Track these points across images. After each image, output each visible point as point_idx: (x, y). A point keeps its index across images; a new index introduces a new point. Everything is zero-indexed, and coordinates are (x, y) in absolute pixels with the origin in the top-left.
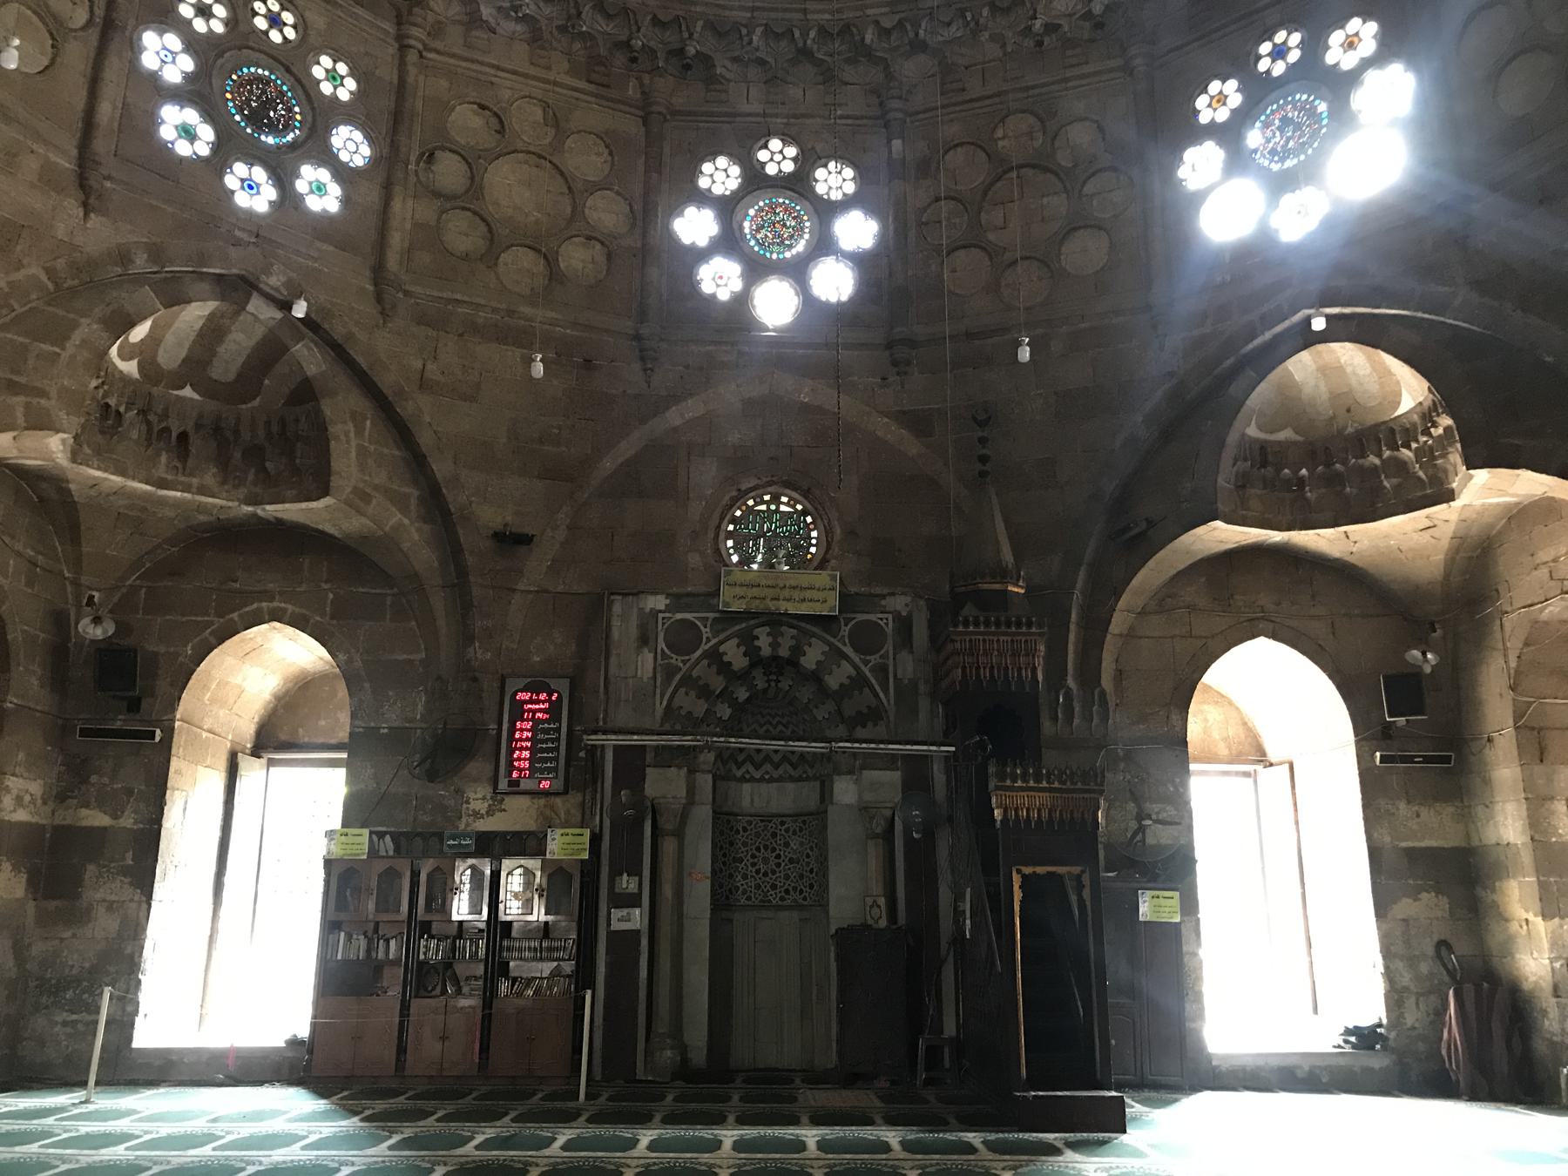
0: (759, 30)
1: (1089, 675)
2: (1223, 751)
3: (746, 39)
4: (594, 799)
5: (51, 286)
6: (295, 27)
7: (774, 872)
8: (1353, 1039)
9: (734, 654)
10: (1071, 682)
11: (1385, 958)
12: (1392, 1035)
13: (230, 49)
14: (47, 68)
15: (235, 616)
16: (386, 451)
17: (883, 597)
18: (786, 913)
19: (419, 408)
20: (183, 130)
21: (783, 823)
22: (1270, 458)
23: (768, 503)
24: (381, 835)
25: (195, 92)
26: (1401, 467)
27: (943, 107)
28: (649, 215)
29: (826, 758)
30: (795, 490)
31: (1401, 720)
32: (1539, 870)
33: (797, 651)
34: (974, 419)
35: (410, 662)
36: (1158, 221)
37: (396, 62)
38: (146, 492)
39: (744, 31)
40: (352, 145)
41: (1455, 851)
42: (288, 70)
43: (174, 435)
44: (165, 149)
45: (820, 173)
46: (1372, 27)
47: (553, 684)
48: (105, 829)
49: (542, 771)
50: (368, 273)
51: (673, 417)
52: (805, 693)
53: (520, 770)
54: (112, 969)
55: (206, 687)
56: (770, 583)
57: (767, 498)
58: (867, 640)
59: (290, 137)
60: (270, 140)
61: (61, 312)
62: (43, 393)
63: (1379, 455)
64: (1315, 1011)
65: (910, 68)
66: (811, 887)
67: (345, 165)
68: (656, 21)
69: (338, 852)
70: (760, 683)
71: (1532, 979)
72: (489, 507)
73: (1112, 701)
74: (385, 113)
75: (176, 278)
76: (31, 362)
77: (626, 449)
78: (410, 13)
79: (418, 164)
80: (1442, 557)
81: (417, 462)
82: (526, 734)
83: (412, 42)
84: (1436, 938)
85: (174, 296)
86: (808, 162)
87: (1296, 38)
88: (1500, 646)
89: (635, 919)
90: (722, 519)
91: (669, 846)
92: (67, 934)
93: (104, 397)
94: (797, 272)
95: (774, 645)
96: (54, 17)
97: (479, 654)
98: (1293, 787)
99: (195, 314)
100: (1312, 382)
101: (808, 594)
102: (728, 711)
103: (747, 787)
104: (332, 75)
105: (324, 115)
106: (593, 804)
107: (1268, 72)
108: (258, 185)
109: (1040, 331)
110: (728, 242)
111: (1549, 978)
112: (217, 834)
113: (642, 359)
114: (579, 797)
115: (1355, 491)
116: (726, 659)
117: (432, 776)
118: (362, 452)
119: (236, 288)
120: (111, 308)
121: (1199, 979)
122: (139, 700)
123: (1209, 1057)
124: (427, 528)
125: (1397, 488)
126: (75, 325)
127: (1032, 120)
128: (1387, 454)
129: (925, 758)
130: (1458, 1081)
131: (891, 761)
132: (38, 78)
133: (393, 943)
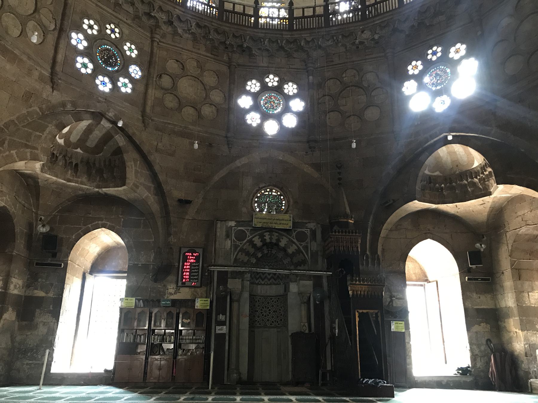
0: (267, 40)
1: (374, 250)
2: (414, 278)
3: (263, 43)
4: (210, 289)
5: (41, 113)
6: (119, 33)
7: (268, 315)
8: (460, 372)
9: (257, 241)
10: (368, 253)
11: (470, 344)
12: (473, 370)
13: (99, 39)
14: (41, 43)
15: (90, 226)
16: (144, 171)
17: (306, 223)
18: (273, 329)
19: (156, 159)
20: (84, 65)
21: (271, 299)
22: (432, 181)
23: (269, 192)
24: (139, 300)
25: (87, 53)
26: (474, 184)
27: (327, 66)
28: (230, 97)
29: (287, 276)
30: (278, 188)
31: (474, 266)
32: (520, 316)
33: (278, 240)
34: (337, 166)
35: (149, 242)
36: (395, 104)
37: (150, 45)
38: (63, 183)
39: (262, 40)
40: (135, 71)
41: (491, 309)
42: (117, 47)
43: (74, 164)
44: (78, 70)
45: (286, 86)
46: (464, 46)
47: (197, 250)
48: (43, 297)
49: (193, 279)
50: (140, 113)
51: (238, 163)
52: (280, 255)
53: (186, 279)
54: (44, 345)
55: (78, 250)
56: (270, 218)
57: (268, 190)
58: (301, 237)
59: (116, 68)
60: (110, 69)
61: (43, 122)
62: (37, 149)
63: (467, 180)
64: (446, 363)
65: (315, 54)
66: (281, 320)
67: (133, 78)
68: (234, 36)
69: (124, 305)
70: (266, 252)
71: (518, 351)
72: (177, 191)
73: (381, 258)
74: (146, 62)
75: (79, 112)
76: (33, 138)
77: (222, 173)
78: (156, 30)
79: (156, 78)
80: (486, 214)
81: (154, 176)
82: (188, 267)
83: (155, 39)
84: (486, 338)
85: (79, 119)
86: (282, 83)
87: (440, 49)
88: (506, 242)
89: (224, 330)
90: (253, 197)
91: (235, 305)
92: (29, 333)
93: (53, 150)
94: (278, 118)
95: (271, 239)
96: (45, 26)
97: (172, 239)
98: (438, 289)
99: (84, 124)
100: (446, 157)
101: (282, 222)
102: (255, 260)
103: (259, 286)
104: (130, 49)
105: (127, 61)
106: (210, 290)
107: (431, 59)
108: (106, 83)
109: (358, 138)
110: (256, 107)
111: (524, 350)
112: (78, 300)
113: (228, 144)
114: (205, 289)
115: (459, 192)
116: (255, 243)
117: (156, 281)
118: (136, 172)
119: (98, 116)
120: (58, 122)
121: (410, 351)
122: (56, 253)
123: (414, 378)
124: (156, 197)
125: (473, 191)
126: (48, 126)
127: (355, 71)
128: (470, 180)
129: (320, 277)
130: (495, 385)
131: (309, 278)
132: (39, 46)
133: (142, 337)
